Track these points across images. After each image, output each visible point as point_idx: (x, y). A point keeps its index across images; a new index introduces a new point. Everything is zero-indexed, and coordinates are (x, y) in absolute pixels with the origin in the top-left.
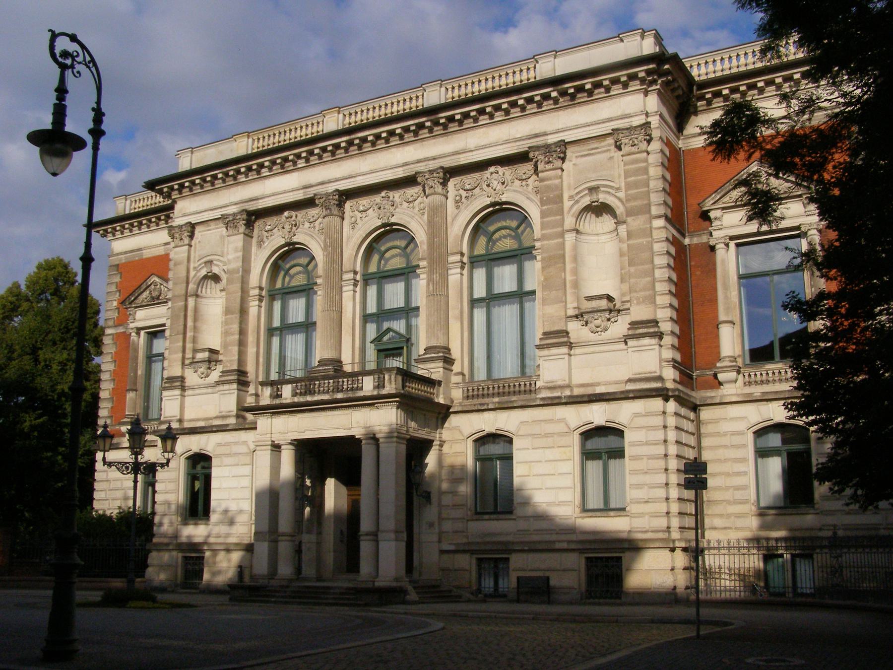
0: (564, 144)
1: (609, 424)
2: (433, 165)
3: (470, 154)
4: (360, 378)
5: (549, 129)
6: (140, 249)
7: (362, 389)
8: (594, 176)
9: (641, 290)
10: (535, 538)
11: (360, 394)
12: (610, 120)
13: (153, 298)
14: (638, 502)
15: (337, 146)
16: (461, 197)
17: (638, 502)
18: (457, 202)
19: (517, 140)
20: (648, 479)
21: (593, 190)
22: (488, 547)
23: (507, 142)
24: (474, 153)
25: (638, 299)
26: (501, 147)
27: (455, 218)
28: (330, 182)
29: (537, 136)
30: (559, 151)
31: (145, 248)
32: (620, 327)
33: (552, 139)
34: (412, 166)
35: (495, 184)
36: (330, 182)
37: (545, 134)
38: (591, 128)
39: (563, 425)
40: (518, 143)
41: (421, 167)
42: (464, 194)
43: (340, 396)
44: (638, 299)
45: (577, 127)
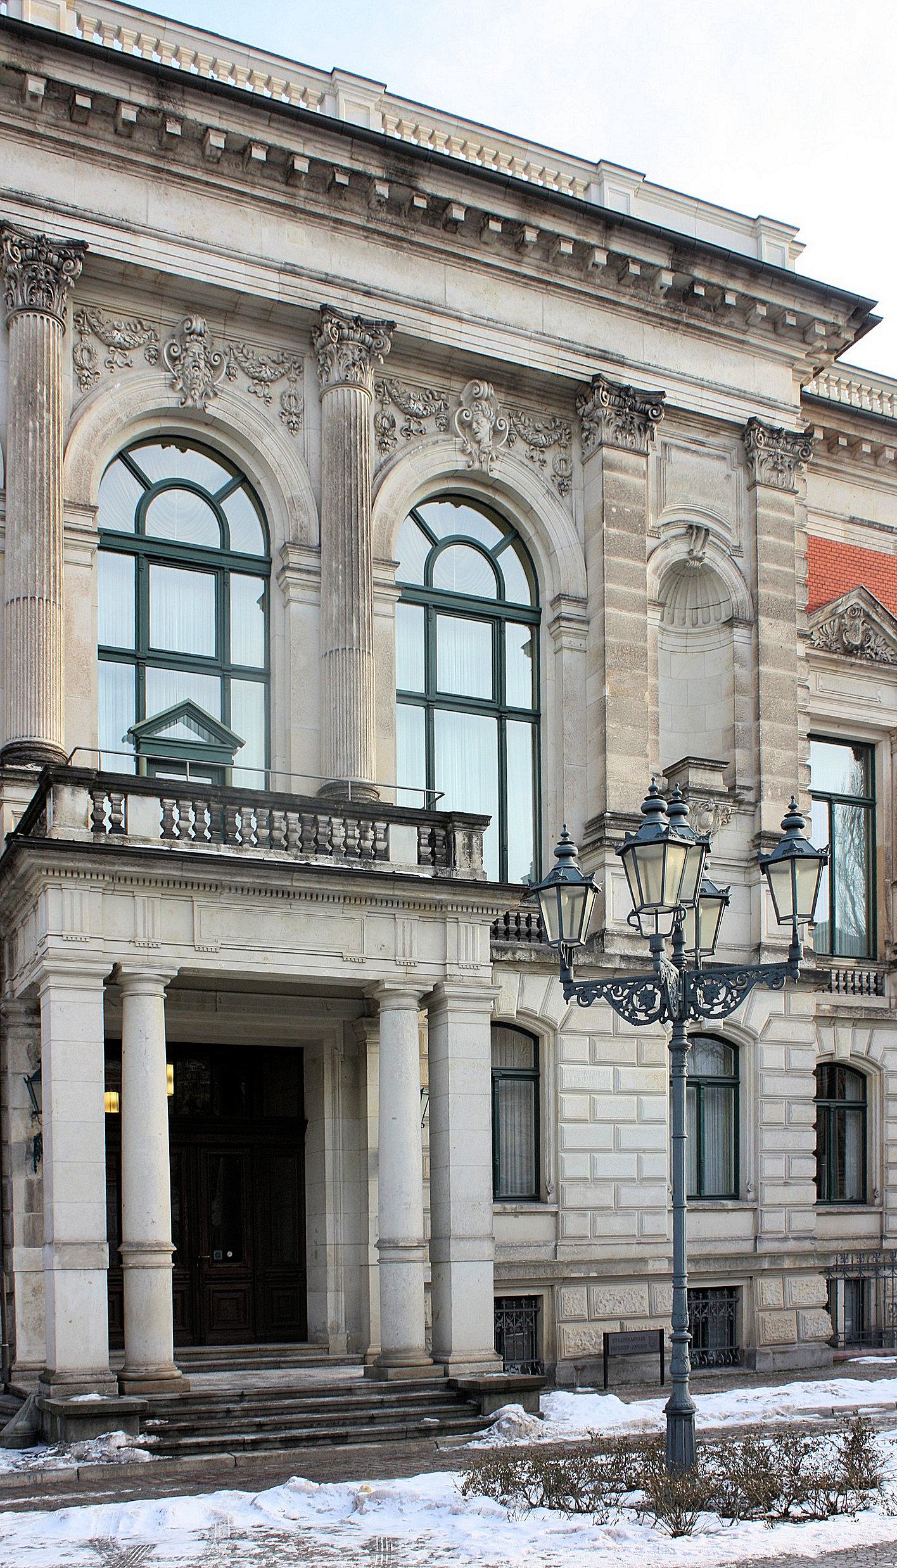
0: (655, 399)
2: (357, 306)
3: (456, 325)
4: (381, 825)
5: (631, 355)
7: (384, 855)
8: (701, 502)
9: (778, 773)
10: (600, 1252)
11: (381, 867)
12: (742, 395)
13: (849, 651)
14: (775, 1181)
15: (107, 107)
16: (393, 425)
17: (775, 1181)
18: (383, 433)
19: (569, 346)
20: (518, 1177)
21: (693, 530)
22: (522, 1274)
23: (543, 338)
24: (465, 327)
25: (774, 788)
26: (526, 344)
27: (383, 471)
28: (51, 207)
29: (604, 356)
30: (642, 411)
33: (630, 379)
34: (305, 283)
35: (484, 430)
36: (51, 207)
37: (621, 362)
38: (706, 394)
40: (562, 354)
41: (332, 297)
42: (400, 422)
43: (324, 861)
44: (774, 788)
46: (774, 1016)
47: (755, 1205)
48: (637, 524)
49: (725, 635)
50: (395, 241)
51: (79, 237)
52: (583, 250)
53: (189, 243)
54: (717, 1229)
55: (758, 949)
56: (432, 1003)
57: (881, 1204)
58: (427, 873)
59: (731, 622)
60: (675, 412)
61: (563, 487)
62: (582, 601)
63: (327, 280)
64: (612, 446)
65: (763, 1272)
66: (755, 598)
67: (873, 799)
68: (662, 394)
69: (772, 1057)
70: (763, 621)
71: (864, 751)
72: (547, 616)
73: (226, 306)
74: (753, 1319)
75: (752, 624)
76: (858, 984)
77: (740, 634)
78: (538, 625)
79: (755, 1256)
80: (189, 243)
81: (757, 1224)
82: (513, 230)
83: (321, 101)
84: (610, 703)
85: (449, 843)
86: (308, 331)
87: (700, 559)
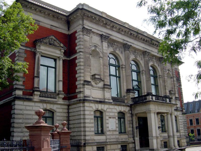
1: (50, 110)
6: (40, 21)
28: (129, 42)
31: (41, 22)
32: (101, 84)
36: (129, 42)
39: (91, 108)
41: (127, 42)
45: (119, 38)
46: (107, 108)
47: (106, 135)
48: (165, 69)
49: (171, 79)
50: (149, 45)
51: (131, 45)
52: (95, 18)
53: (138, 45)
54: (101, 138)
55: (177, 108)
56: (171, 114)
57: (106, 134)
58: (170, 103)
59: (171, 78)
60: (93, 32)
61: (159, 65)
62: (161, 76)
63: (146, 49)
64: (86, 35)
65: (108, 144)
66: (173, 76)
67: (56, 67)
68: (92, 30)
69: (180, 118)
70: (104, 57)
71: (55, 60)
72: (121, 67)
73: (77, 27)
74: (181, 144)
75: (173, 78)
76: (54, 97)
77: (172, 79)
78: (119, 67)
79: (106, 142)
80: (138, 45)
81: (180, 134)
82: (92, 17)
83: (143, 33)
84: (166, 85)
85: (170, 100)
86: (144, 53)
87: (96, 49)
